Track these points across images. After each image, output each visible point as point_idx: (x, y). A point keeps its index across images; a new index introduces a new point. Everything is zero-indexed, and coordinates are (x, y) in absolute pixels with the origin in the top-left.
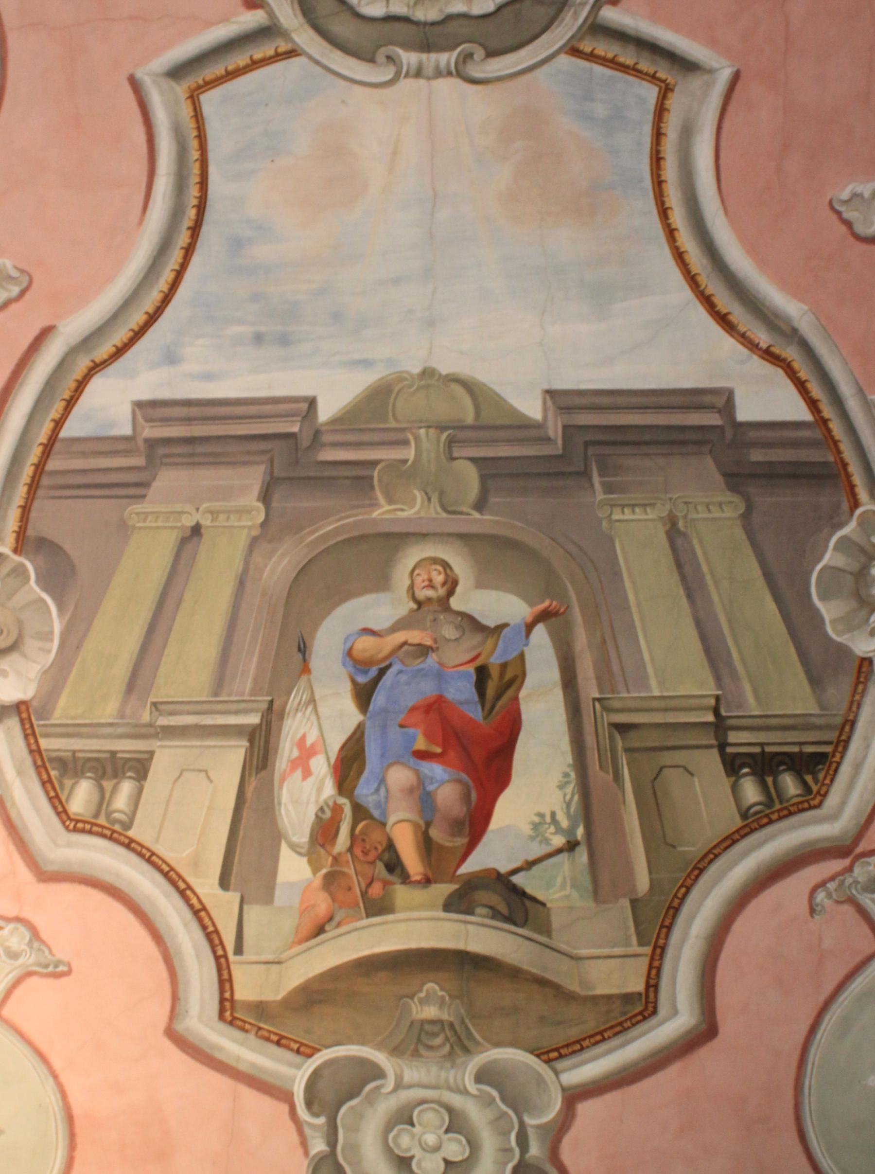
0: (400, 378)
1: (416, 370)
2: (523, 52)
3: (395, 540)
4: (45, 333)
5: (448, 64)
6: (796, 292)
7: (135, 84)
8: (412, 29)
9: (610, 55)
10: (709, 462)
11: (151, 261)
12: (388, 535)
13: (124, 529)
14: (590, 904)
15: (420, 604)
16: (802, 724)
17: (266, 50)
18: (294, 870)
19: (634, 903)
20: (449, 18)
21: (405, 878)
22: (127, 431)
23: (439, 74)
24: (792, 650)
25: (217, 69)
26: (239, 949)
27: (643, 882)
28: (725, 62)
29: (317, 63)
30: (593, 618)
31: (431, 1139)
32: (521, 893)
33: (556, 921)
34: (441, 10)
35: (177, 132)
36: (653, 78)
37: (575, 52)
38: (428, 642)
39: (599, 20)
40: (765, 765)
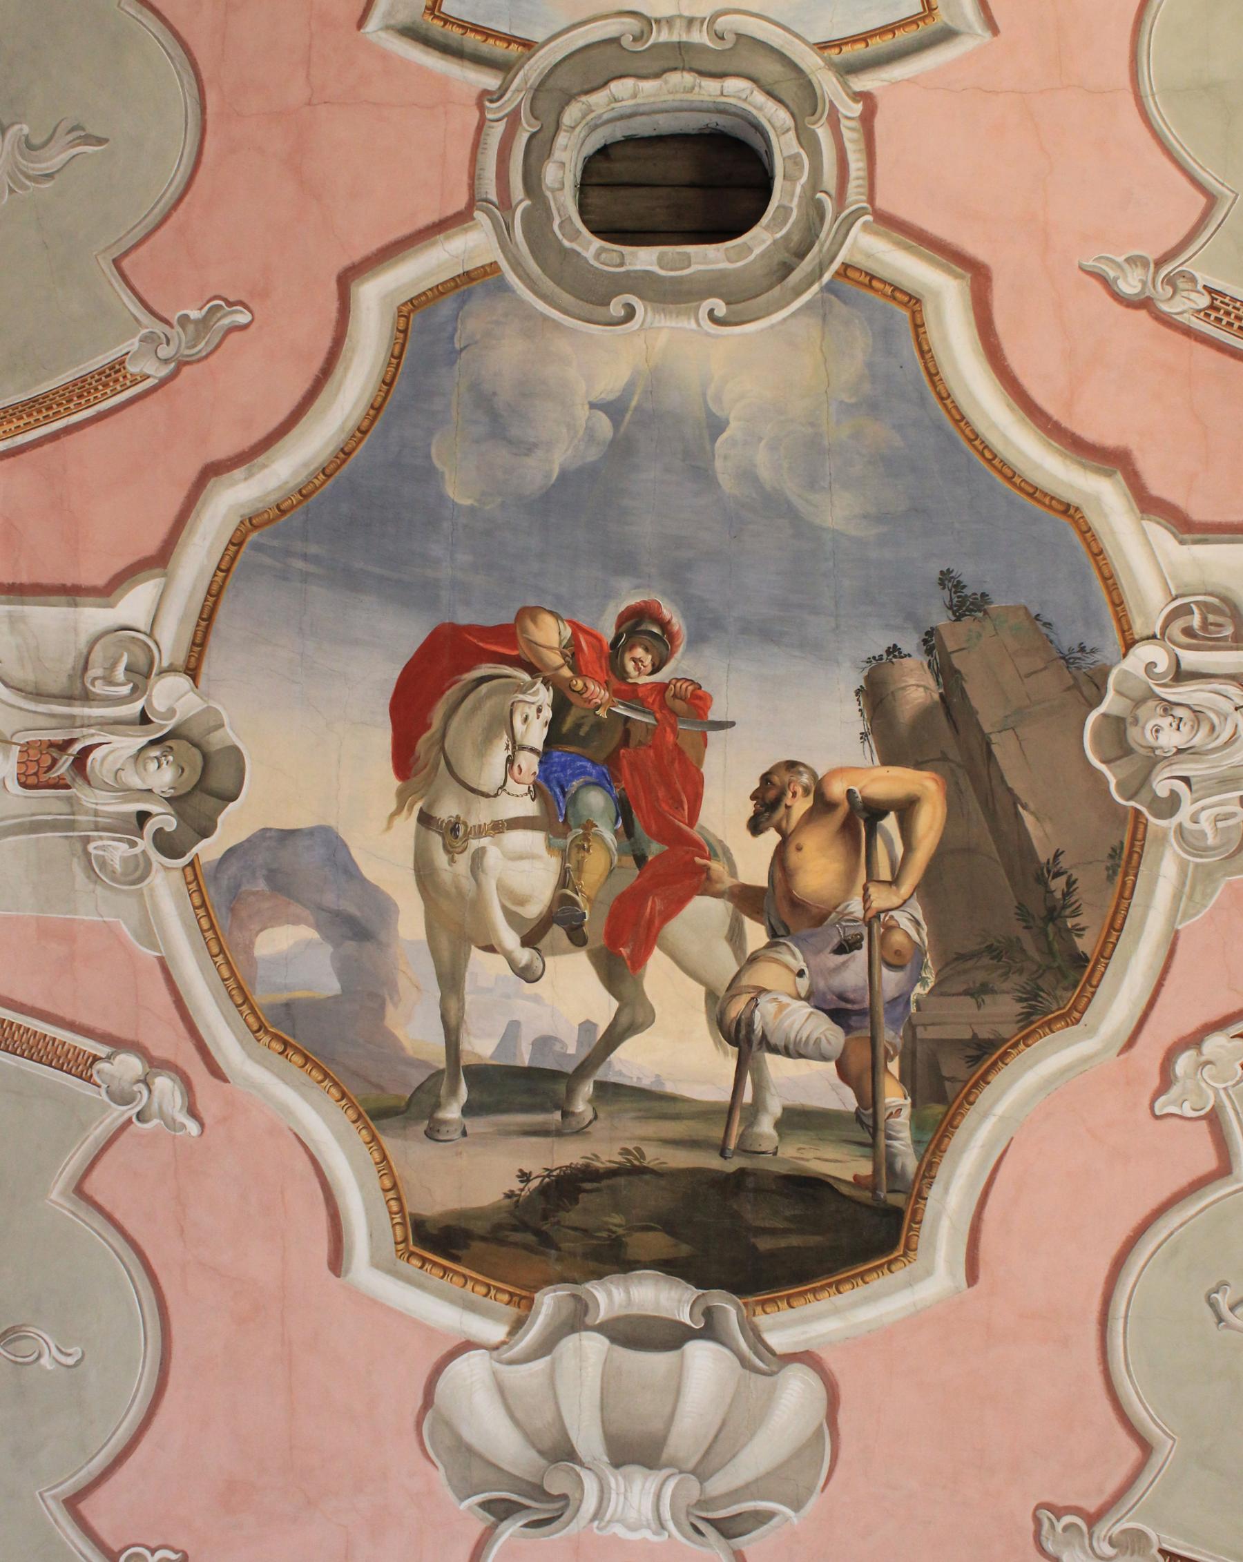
2: (581, 43)
5: (659, 31)
7: (992, 25)
8: (696, 65)
9: (491, 41)
11: (111, 1459)
17: (851, 52)
20: (657, 76)
23: (670, 21)
25: (903, 36)
28: (373, 38)
29: (797, 36)
34: (666, 82)
36: (446, 20)
37: (527, 44)
39: (501, 76)
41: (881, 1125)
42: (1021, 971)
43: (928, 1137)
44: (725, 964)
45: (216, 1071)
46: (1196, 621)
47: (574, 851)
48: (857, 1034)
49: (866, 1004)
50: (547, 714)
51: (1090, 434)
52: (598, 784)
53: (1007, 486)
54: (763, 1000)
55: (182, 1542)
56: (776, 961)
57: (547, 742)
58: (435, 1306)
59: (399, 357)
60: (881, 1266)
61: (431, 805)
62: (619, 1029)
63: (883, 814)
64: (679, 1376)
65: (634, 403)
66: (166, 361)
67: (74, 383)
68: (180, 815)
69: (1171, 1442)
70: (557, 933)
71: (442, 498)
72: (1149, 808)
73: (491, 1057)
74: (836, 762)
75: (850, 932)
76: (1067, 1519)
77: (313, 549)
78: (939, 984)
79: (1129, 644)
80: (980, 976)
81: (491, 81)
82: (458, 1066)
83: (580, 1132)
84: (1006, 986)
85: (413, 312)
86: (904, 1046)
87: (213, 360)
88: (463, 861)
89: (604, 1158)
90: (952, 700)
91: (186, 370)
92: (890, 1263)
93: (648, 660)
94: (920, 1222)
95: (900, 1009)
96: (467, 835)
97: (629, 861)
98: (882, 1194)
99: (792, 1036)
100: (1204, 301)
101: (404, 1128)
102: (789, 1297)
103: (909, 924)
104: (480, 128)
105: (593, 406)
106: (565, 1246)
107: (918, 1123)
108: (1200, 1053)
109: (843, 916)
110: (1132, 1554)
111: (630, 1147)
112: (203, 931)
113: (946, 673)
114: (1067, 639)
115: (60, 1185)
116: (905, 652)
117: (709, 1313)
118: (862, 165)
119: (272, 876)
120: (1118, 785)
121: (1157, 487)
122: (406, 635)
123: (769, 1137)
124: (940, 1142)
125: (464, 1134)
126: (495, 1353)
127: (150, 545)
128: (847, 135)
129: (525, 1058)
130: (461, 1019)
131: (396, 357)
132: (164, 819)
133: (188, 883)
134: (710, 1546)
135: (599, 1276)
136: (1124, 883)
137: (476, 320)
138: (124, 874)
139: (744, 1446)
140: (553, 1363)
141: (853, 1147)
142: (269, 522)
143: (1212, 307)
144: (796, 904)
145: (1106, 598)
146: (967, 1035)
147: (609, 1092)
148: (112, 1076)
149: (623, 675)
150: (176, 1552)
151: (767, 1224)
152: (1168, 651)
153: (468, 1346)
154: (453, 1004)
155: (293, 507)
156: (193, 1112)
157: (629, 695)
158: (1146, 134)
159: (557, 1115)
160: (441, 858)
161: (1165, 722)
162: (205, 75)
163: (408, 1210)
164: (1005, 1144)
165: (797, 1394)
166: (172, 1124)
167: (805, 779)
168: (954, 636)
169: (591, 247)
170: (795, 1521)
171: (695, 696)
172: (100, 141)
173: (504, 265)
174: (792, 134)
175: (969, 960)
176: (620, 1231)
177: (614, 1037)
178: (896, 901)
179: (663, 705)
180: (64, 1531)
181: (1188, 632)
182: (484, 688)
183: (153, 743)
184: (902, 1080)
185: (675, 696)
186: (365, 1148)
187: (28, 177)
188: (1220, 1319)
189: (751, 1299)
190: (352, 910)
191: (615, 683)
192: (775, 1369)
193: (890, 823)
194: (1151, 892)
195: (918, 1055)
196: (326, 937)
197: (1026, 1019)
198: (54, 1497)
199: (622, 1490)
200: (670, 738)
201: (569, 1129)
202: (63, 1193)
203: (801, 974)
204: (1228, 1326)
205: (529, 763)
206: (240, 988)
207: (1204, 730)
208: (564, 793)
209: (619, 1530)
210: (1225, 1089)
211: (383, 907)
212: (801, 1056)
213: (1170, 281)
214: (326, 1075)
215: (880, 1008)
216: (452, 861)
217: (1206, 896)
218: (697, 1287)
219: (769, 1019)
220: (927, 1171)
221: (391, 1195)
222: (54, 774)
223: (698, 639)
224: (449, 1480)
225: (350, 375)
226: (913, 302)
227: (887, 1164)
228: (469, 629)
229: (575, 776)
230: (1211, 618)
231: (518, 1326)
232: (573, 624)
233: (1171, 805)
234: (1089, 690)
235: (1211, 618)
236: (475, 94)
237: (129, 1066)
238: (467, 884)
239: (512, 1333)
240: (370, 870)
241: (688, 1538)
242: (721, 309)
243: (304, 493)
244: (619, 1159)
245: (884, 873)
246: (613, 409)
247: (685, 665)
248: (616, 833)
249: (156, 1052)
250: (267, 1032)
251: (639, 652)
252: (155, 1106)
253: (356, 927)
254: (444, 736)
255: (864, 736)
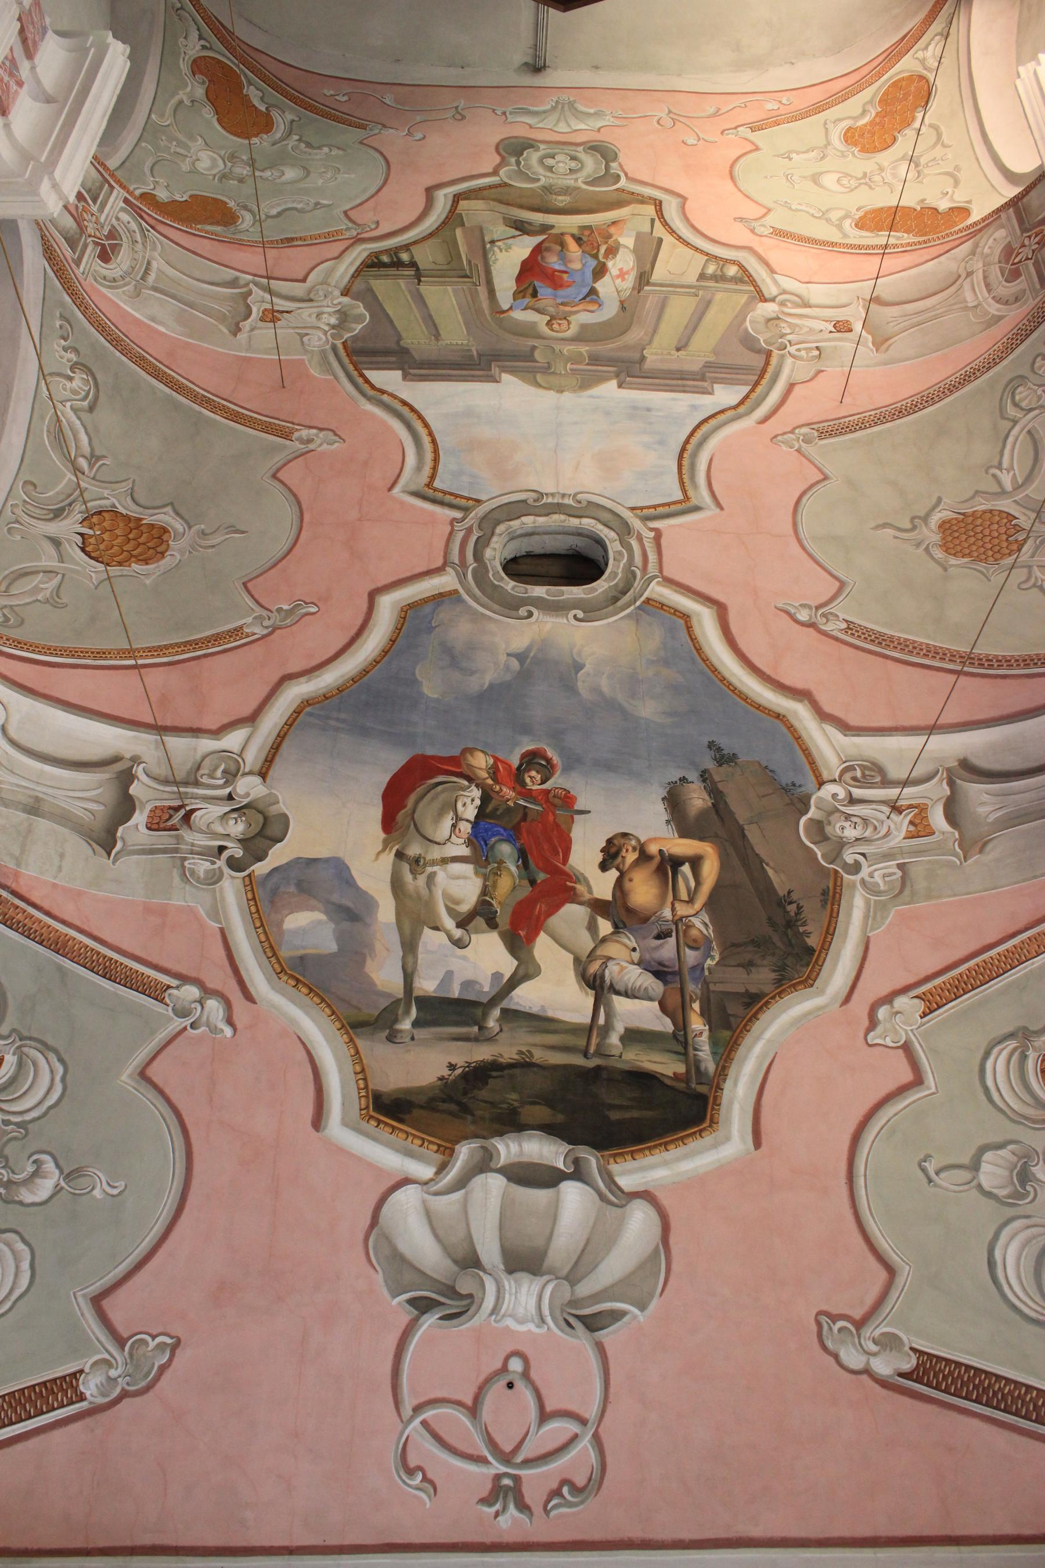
0: (575, 391)
1: (566, 393)
3: (577, 339)
4: (764, 421)
6: (366, 413)
10: (417, 357)
12: (581, 341)
13: (715, 352)
14: (484, 226)
15: (565, 318)
16: (377, 277)
18: (627, 240)
19: (463, 225)
21: (573, 236)
22: (715, 386)
23: (553, 495)
24: (380, 298)
25: (673, 508)
26: (653, 221)
27: (459, 232)
30: (479, 311)
31: (561, 165)
32: (517, 229)
33: (501, 221)
35: (695, 486)
36: (435, 490)
37: (478, 501)
38: (561, 307)
40: (398, 264)
41: (690, 1042)
42: (773, 954)
43: (721, 1051)
44: (587, 943)
45: (249, 997)
46: (859, 774)
47: (492, 876)
48: (670, 986)
49: (677, 968)
50: (478, 802)
51: (787, 682)
52: (507, 841)
53: (743, 703)
54: (610, 964)
55: (178, 1331)
56: (617, 941)
57: (476, 817)
58: (384, 1154)
59: (400, 629)
60: (695, 1133)
61: (404, 847)
62: (518, 977)
63: (682, 864)
64: (555, 1208)
65: (532, 655)
66: (267, 627)
67: (213, 635)
68: (246, 849)
69: (908, 1267)
70: (479, 921)
71: (421, 694)
72: (842, 869)
73: (435, 991)
74: (652, 834)
75: (663, 927)
76: (841, 1324)
77: (343, 716)
78: (722, 959)
79: (821, 784)
80: (748, 957)
81: (458, 515)
82: (411, 995)
83: (491, 1040)
84: (765, 962)
85: (408, 612)
86: (702, 994)
87: (294, 628)
88: (422, 880)
89: (506, 1056)
90: (719, 805)
91: (278, 632)
92: (701, 1131)
93: (538, 777)
94: (719, 1105)
95: (698, 973)
96: (425, 865)
97: (526, 883)
98: (693, 1086)
99: (630, 986)
100: (844, 626)
101: (373, 1034)
102: (632, 1152)
103: (701, 924)
104: (451, 533)
105: (508, 655)
106: (478, 1113)
107: (714, 1042)
108: (892, 1007)
109: (659, 919)
110: (891, 1350)
111: (524, 1050)
112: (251, 914)
113: (715, 792)
114: (785, 779)
115: (129, 1071)
116: (690, 780)
117: (576, 1162)
118: (655, 557)
119: (299, 884)
120: (822, 855)
121: (827, 708)
122: (396, 760)
123: (616, 1046)
124: (728, 1056)
125: (413, 1039)
126: (425, 1187)
127: (247, 711)
128: (647, 544)
129: (455, 993)
130: (415, 969)
131: (398, 629)
132: (236, 851)
133: (245, 886)
134: (578, 1337)
135: (501, 1134)
136: (832, 909)
137: (444, 614)
138: (206, 879)
139: (603, 1259)
140: (467, 1193)
141: (672, 1055)
142: (318, 702)
143: (848, 628)
144: (630, 911)
145: (805, 760)
146: (743, 990)
147: (511, 1015)
148: (178, 998)
149: (523, 784)
150: (172, 1337)
151: (616, 1102)
152: (845, 789)
153: (406, 1181)
154: (410, 960)
155: (333, 696)
156: (230, 1021)
157: (528, 795)
158: (806, 556)
159: (476, 1029)
160: (408, 877)
161: (847, 824)
162: (304, 507)
163: (371, 1087)
164: (772, 1056)
165: (639, 1223)
166: (214, 1030)
167: (633, 842)
168: (718, 774)
169: (509, 585)
170: (641, 1319)
171: (566, 796)
172: (243, 532)
173: (461, 591)
174: (618, 542)
175: (739, 948)
176: (516, 1104)
177: (514, 982)
178: (692, 912)
179: (547, 801)
180: (87, 1322)
181: (854, 779)
182: (440, 788)
183: (233, 810)
184: (702, 1014)
185: (554, 796)
186: (345, 1046)
187: (201, 547)
188: (930, 1181)
189: (607, 1153)
190: (350, 904)
191: (518, 787)
192: (624, 1202)
193: (686, 868)
194: (849, 915)
195: (712, 1001)
196: (331, 919)
197: (779, 982)
198: (84, 1296)
199: (514, 1291)
200: (551, 818)
201: (483, 1037)
202: (130, 1076)
203: (634, 950)
204: (936, 1185)
205: (466, 828)
206: (271, 947)
207: (870, 829)
208: (486, 845)
209: (510, 1322)
210: (912, 1030)
211: (369, 903)
212: (636, 997)
213: (824, 615)
214: (323, 1000)
215: (686, 971)
216: (415, 878)
217: (884, 918)
218: (569, 1143)
219: (615, 975)
220: (722, 1071)
221: (360, 1076)
222: (170, 823)
223: (567, 769)
224: (385, 1281)
225: (372, 636)
226: (686, 617)
227: (695, 1067)
228: (433, 757)
229: (493, 835)
230: (867, 773)
231: (442, 1168)
232: (494, 757)
233: (856, 868)
234: (800, 806)
235: (867, 773)
236: (449, 520)
237: (192, 992)
238: (424, 892)
239: (437, 1173)
240: (362, 883)
241: (562, 1331)
242: (580, 614)
243: (340, 690)
244: (516, 1057)
245: (684, 895)
246: (521, 657)
247: (560, 781)
248: (518, 867)
249: (210, 985)
250: (286, 974)
251: (533, 773)
252: (204, 1018)
253: (352, 913)
254: (414, 812)
255: (668, 822)
